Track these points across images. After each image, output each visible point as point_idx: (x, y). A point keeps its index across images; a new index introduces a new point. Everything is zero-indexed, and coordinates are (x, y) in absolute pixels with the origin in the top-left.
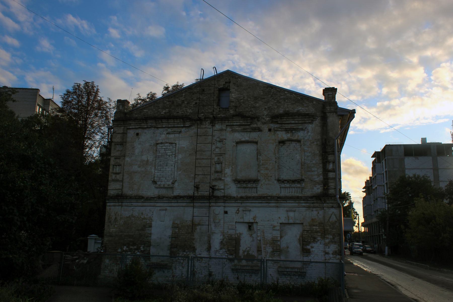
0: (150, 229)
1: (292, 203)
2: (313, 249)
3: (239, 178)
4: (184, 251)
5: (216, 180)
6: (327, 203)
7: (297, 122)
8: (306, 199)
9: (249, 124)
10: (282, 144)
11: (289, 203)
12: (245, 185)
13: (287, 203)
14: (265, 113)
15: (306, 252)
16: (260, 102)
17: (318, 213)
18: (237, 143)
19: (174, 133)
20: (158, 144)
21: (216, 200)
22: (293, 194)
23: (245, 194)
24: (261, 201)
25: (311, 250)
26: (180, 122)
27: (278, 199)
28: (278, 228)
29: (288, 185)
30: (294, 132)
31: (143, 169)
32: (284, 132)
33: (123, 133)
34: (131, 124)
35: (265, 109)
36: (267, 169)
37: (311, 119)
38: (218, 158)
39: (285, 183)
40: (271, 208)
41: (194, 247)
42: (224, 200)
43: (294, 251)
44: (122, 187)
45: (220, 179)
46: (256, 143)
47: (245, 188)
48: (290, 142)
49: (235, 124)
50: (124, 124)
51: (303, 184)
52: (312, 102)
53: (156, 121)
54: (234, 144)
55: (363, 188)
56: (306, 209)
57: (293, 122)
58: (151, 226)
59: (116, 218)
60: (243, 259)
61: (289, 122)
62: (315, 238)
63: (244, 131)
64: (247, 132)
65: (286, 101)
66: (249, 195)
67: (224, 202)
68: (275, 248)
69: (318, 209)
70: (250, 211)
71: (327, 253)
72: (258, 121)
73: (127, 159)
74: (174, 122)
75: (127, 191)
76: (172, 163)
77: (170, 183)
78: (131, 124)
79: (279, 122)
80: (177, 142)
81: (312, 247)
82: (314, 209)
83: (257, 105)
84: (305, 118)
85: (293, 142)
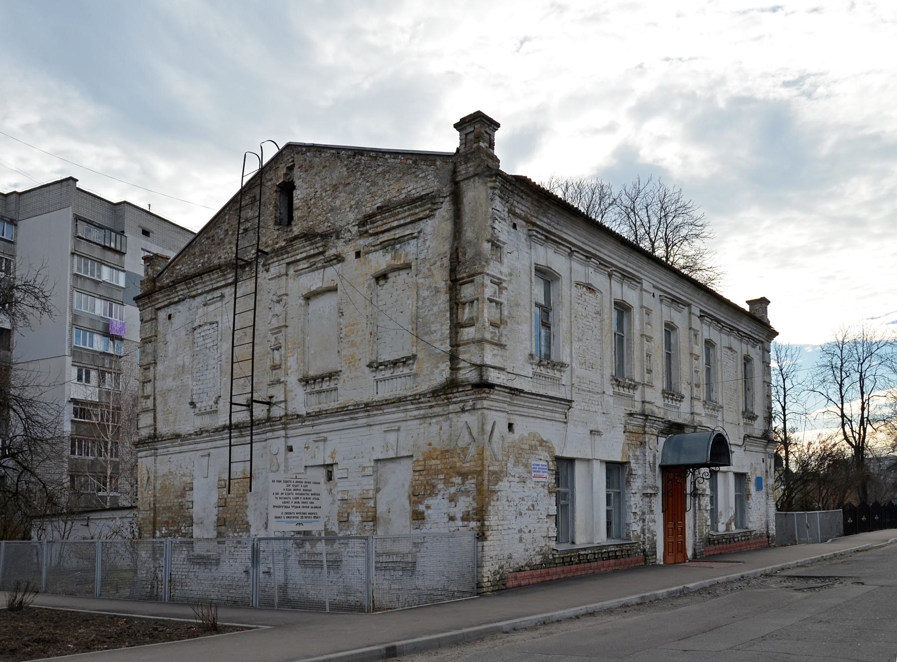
0: (191, 492)
1: (394, 413)
2: (430, 511)
3: (312, 373)
4: (235, 531)
5: (272, 384)
6: (455, 403)
7: (402, 222)
8: (416, 399)
9: (321, 249)
10: (382, 282)
11: (389, 413)
12: (317, 388)
13: (384, 414)
14: (351, 216)
15: (418, 517)
16: (342, 194)
17: (441, 429)
18: (308, 298)
19: (213, 301)
20: (195, 329)
21: (271, 426)
22: (397, 392)
23: (319, 406)
24: (340, 418)
25: (426, 513)
26: (219, 277)
27: (368, 407)
28: (369, 471)
29: (388, 373)
30: (398, 246)
31: (179, 383)
32: (381, 252)
33: (152, 319)
34: (157, 299)
35: (351, 207)
36: (353, 344)
37: (426, 207)
38: (276, 338)
39: (409, 365)
40: (360, 430)
41: (248, 523)
42: (282, 424)
43: (398, 521)
44: (155, 421)
45: (279, 382)
46: (334, 290)
47: (319, 392)
48: (396, 273)
49: (298, 257)
50: (150, 302)
51: (415, 366)
52: (435, 164)
53: (186, 284)
54: (302, 302)
55: (748, 302)
56: (418, 421)
57: (395, 224)
58: (192, 489)
59: (149, 478)
60: (320, 540)
61: (388, 226)
62: (434, 487)
63: (313, 268)
64: (317, 269)
65: (387, 175)
66: (324, 407)
67: (284, 429)
68: (364, 515)
69: (441, 418)
70: (325, 440)
71: (452, 519)
72: (338, 238)
73: (160, 367)
74: (196, 285)
75: (163, 429)
76: (214, 362)
77: (211, 403)
78: (157, 299)
79: (370, 232)
80: (219, 319)
81: (428, 507)
82: (434, 420)
83: (338, 202)
84: (416, 207)
85: (401, 272)
